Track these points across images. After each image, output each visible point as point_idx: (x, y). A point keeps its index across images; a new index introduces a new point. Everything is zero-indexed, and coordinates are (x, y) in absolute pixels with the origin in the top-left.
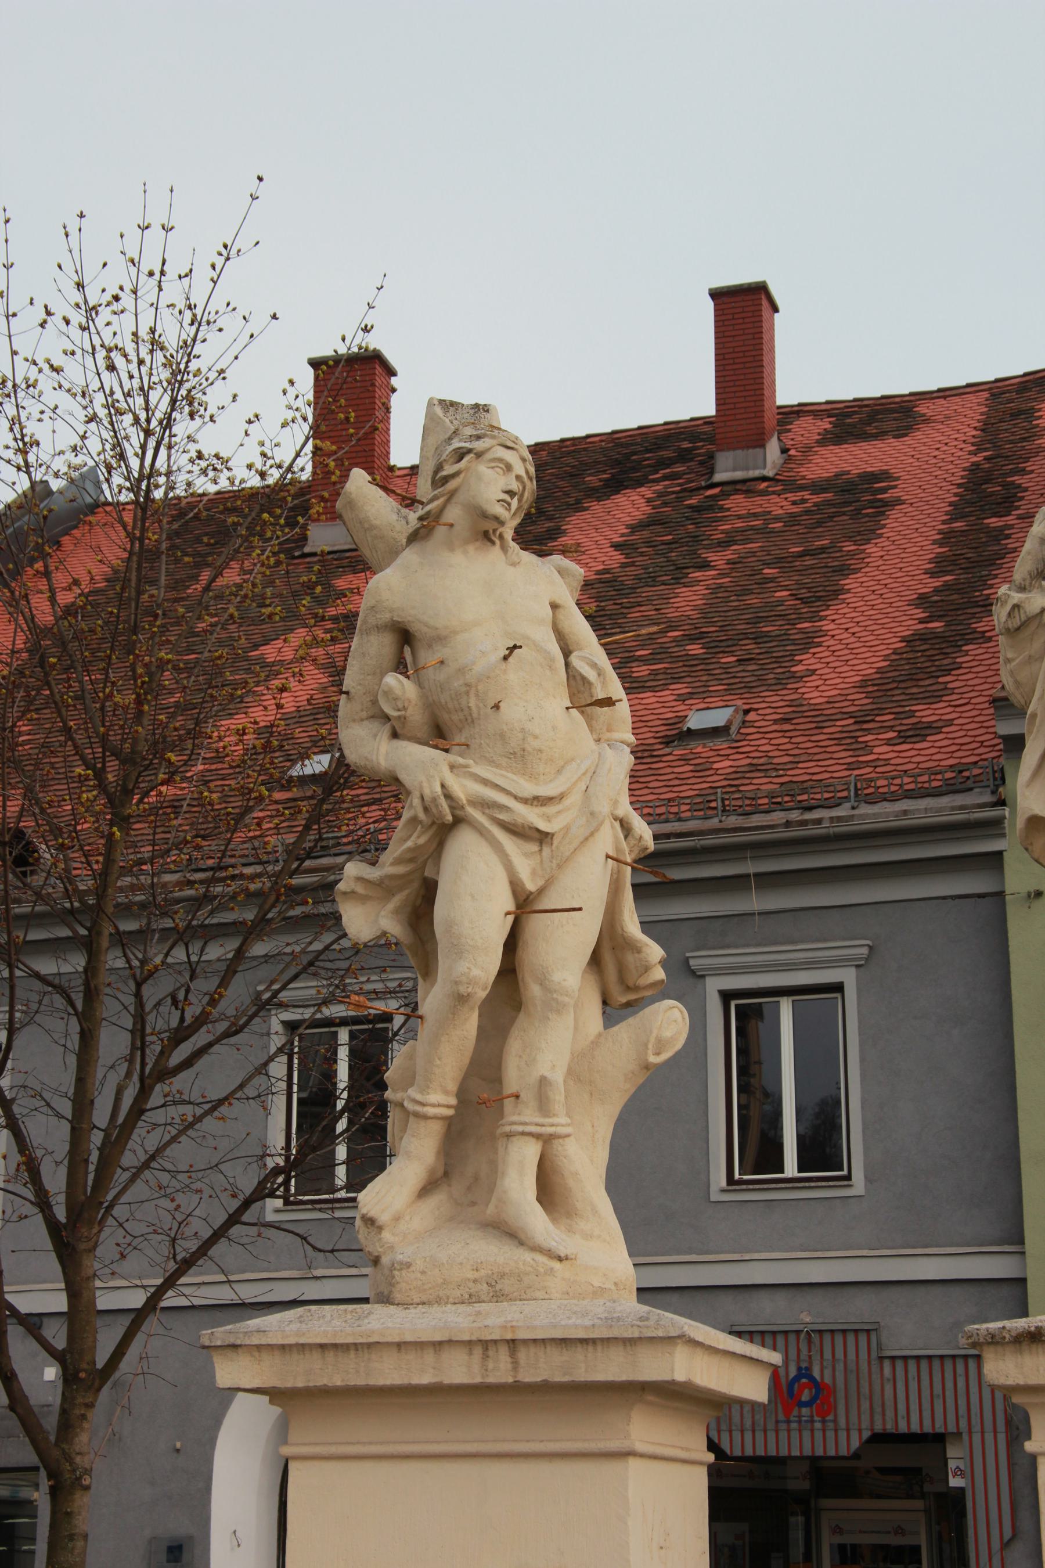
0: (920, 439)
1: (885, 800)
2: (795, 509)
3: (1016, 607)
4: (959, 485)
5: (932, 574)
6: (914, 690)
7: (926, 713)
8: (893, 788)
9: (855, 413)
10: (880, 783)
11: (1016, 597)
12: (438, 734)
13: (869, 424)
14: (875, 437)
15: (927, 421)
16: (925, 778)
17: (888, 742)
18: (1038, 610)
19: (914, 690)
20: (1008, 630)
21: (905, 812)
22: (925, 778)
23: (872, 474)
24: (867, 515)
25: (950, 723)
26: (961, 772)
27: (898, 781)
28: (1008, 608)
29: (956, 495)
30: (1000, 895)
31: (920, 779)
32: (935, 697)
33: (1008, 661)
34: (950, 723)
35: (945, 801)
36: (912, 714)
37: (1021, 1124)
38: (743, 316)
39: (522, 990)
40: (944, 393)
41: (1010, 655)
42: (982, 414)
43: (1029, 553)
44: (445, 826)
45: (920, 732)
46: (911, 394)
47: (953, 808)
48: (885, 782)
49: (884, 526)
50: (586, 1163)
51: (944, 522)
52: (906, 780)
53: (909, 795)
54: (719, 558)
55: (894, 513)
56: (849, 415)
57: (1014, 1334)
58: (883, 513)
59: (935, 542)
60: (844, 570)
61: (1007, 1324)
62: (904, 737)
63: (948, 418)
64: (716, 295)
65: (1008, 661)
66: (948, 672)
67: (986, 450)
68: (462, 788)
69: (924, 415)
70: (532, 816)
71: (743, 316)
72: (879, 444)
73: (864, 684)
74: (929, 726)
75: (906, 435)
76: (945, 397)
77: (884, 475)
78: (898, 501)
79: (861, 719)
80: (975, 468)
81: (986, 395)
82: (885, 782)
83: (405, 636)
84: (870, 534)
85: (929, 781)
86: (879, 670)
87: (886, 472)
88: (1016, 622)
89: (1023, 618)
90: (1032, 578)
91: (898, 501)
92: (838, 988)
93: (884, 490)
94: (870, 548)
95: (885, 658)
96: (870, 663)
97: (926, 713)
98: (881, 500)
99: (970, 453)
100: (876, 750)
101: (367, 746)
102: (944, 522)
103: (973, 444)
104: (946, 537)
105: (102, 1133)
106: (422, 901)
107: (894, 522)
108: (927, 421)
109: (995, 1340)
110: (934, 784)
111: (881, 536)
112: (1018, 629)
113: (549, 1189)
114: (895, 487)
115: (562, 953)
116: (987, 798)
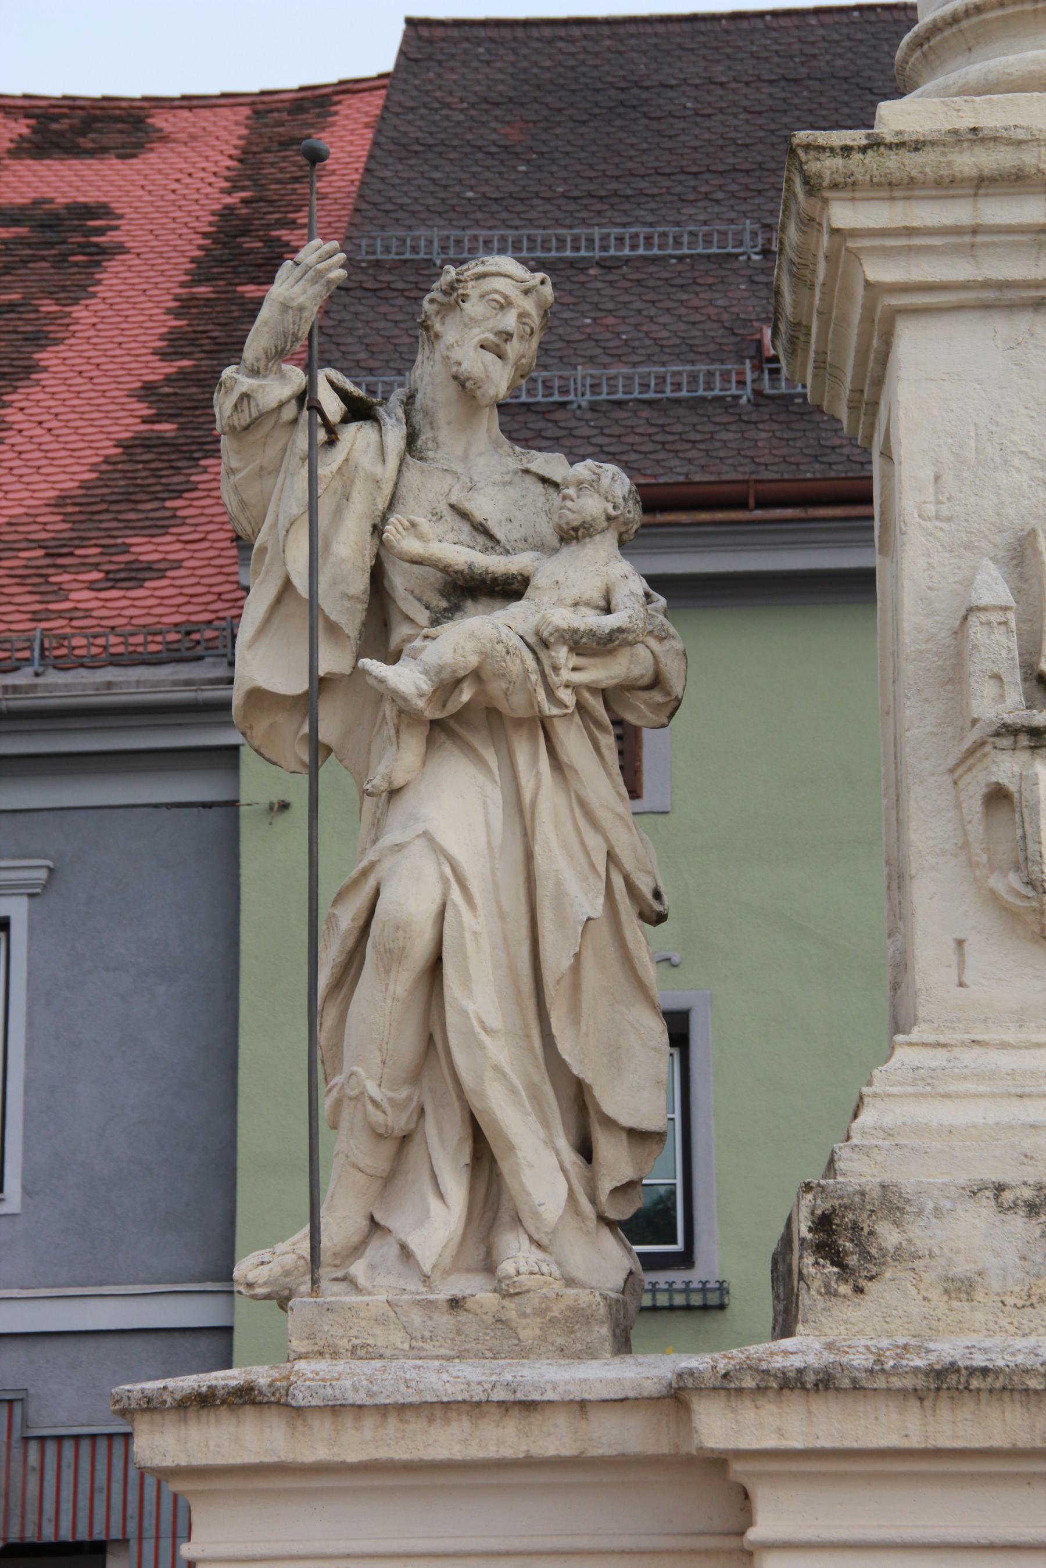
0: (153, 163)
1: (82, 666)
3: (245, 396)
4: (205, 235)
5: (164, 355)
6: (132, 516)
7: (146, 549)
8: (94, 650)
9: (64, 116)
10: (75, 642)
11: (246, 383)
13: (83, 134)
14: (91, 153)
15: (165, 139)
16: (139, 639)
17: (91, 586)
18: (274, 404)
19: (132, 516)
20: (233, 428)
21: (109, 685)
22: (139, 639)
23: (85, 206)
24: (76, 264)
25: (178, 564)
26: (188, 633)
27: (101, 641)
28: (234, 397)
29: (200, 247)
30: (233, 804)
31: (132, 640)
32: (158, 527)
33: (232, 471)
34: (178, 564)
35: (164, 672)
36: (126, 549)
37: (241, 1118)
39: (508, 1178)
40: (190, 103)
41: (234, 464)
42: (240, 137)
43: (265, 323)
45: (135, 574)
46: (145, 99)
47: (175, 683)
48: (83, 642)
49: (99, 282)
51: (182, 285)
52: (113, 640)
53: (116, 661)
55: (114, 265)
56: (56, 118)
57: (178, 1396)
58: (98, 264)
59: (169, 311)
60: (40, 339)
61: (170, 1383)
62: (112, 581)
63: (193, 137)
65: (232, 471)
66: (179, 494)
67: (243, 189)
69: (160, 130)
72: (76, 164)
73: (60, 502)
74: (149, 567)
75: (134, 156)
76: (190, 108)
77: (102, 210)
78: (121, 249)
79: (56, 551)
80: (227, 213)
81: (246, 111)
82: (83, 642)
84: (77, 291)
85: (145, 644)
86: (84, 485)
87: (105, 206)
88: (244, 419)
89: (255, 414)
90: (268, 359)
91: (121, 249)
93: (101, 231)
94: (78, 311)
95: (93, 468)
96: (72, 473)
97: (146, 549)
98: (96, 245)
99: (222, 191)
100: (73, 596)
102: (182, 285)
103: (227, 179)
104: (185, 306)
107: (113, 276)
108: (165, 139)
109: (151, 1406)
110: (153, 648)
111: (94, 295)
112: (247, 428)
114: (116, 228)
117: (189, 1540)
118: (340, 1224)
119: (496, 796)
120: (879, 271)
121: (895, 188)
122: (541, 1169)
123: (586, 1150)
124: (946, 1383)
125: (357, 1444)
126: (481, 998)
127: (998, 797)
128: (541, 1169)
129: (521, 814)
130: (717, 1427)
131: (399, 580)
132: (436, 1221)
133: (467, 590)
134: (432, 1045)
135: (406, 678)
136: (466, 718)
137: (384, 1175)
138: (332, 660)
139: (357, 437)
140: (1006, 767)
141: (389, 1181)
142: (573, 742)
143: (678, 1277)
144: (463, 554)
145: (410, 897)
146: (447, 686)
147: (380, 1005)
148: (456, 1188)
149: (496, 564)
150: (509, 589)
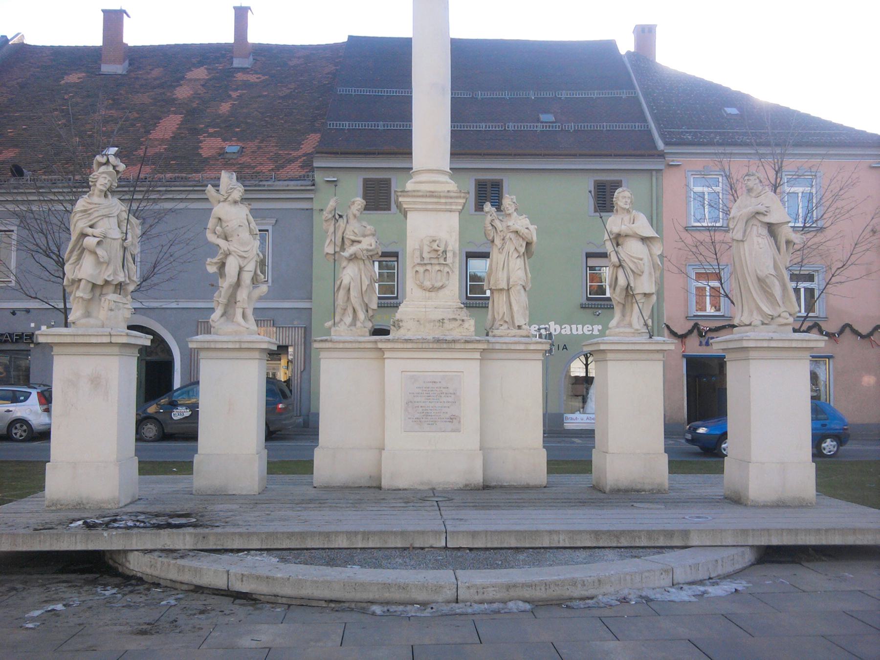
2: (258, 80)
12: (226, 239)
38: (241, 14)
44: (227, 254)
50: (249, 312)
54: (234, 95)
64: (235, 8)
68: (232, 248)
70: (244, 254)
71: (241, 14)
83: (220, 219)
92: (267, 231)
101: (211, 238)
105: (524, 453)
106: (222, 265)
113: (244, 316)
115: (247, 277)
116: (310, 183)
117: (592, 432)
118: (337, 319)
119: (357, 270)
120: (405, 206)
121: (408, 196)
122: (361, 315)
123: (367, 311)
124: (407, 341)
125: (341, 345)
126: (353, 293)
127: (417, 271)
128: (361, 315)
129: (360, 270)
130: (380, 345)
131: (345, 240)
132: (348, 319)
133: (353, 241)
134: (349, 298)
135: (346, 254)
136: (353, 258)
137: (231, 588)
138: (338, 249)
139: (340, 220)
140: (417, 268)
141: (343, 314)
142: (367, 262)
143: (395, 301)
144: (353, 238)
145: (346, 281)
146: (351, 255)
147: (342, 294)
148: (351, 316)
149: (357, 239)
150: (359, 242)
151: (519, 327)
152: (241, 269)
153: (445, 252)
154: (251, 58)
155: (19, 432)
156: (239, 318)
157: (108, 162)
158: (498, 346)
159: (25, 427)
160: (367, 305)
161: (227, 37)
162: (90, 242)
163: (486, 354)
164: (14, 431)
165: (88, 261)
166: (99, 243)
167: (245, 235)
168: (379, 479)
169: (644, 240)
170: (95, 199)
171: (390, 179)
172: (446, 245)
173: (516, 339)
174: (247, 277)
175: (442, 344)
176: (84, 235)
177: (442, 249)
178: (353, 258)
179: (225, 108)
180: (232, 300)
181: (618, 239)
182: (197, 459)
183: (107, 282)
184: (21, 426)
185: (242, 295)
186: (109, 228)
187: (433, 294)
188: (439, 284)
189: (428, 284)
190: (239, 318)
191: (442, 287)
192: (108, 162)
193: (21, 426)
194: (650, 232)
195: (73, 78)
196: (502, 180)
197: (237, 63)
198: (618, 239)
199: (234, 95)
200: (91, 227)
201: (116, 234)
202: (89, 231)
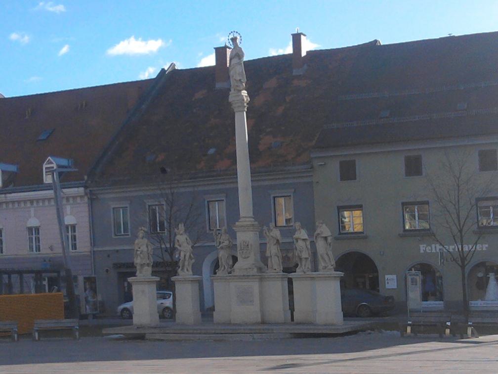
38: (297, 39)
71: (297, 39)
113: (187, 270)
115: (187, 258)
132: (223, 268)
136: (222, 248)
151: (275, 269)
152: (185, 256)
153: (248, 245)
154: (305, 67)
155: (168, 314)
156: (185, 270)
157: (142, 230)
158: (266, 277)
159: (169, 312)
160: (228, 264)
161: (289, 50)
162: (139, 252)
163: (261, 279)
164: (165, 313)
165: (139, 258)
166: (141, 253)
167: (185, 244)
168: (230, 321)
169: (304, 240)
170: (141, 240)
171: (355, 161)
172: (249, 242)
173: (273, 274)
174: (187, 258)
175: (246, 277)
176: (137, 250)
177: (247, 244)
178: (222, 248)
179: (280, 110)
180: (183, 266)
181: (297, 240)
182: (214, 319)
183: (144, 264)
184: (168, 311)
185: (186, 263)
186: (144, 248)
187: (245, 259)
188: (246, 256)
189: (243, 256)
190: (185, 270)
191: (248, 257)
192: (142, 230)
193: (168, 311)
194: (306, 237)
195: (199, 95)
196: (421, 156)
197: (295, 72)
198: (297, 240)
199: (288, 99)
200: (139, 248)
201: (145, 249)
202: (139, 249)
